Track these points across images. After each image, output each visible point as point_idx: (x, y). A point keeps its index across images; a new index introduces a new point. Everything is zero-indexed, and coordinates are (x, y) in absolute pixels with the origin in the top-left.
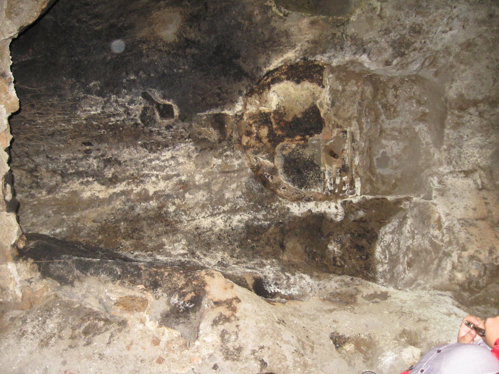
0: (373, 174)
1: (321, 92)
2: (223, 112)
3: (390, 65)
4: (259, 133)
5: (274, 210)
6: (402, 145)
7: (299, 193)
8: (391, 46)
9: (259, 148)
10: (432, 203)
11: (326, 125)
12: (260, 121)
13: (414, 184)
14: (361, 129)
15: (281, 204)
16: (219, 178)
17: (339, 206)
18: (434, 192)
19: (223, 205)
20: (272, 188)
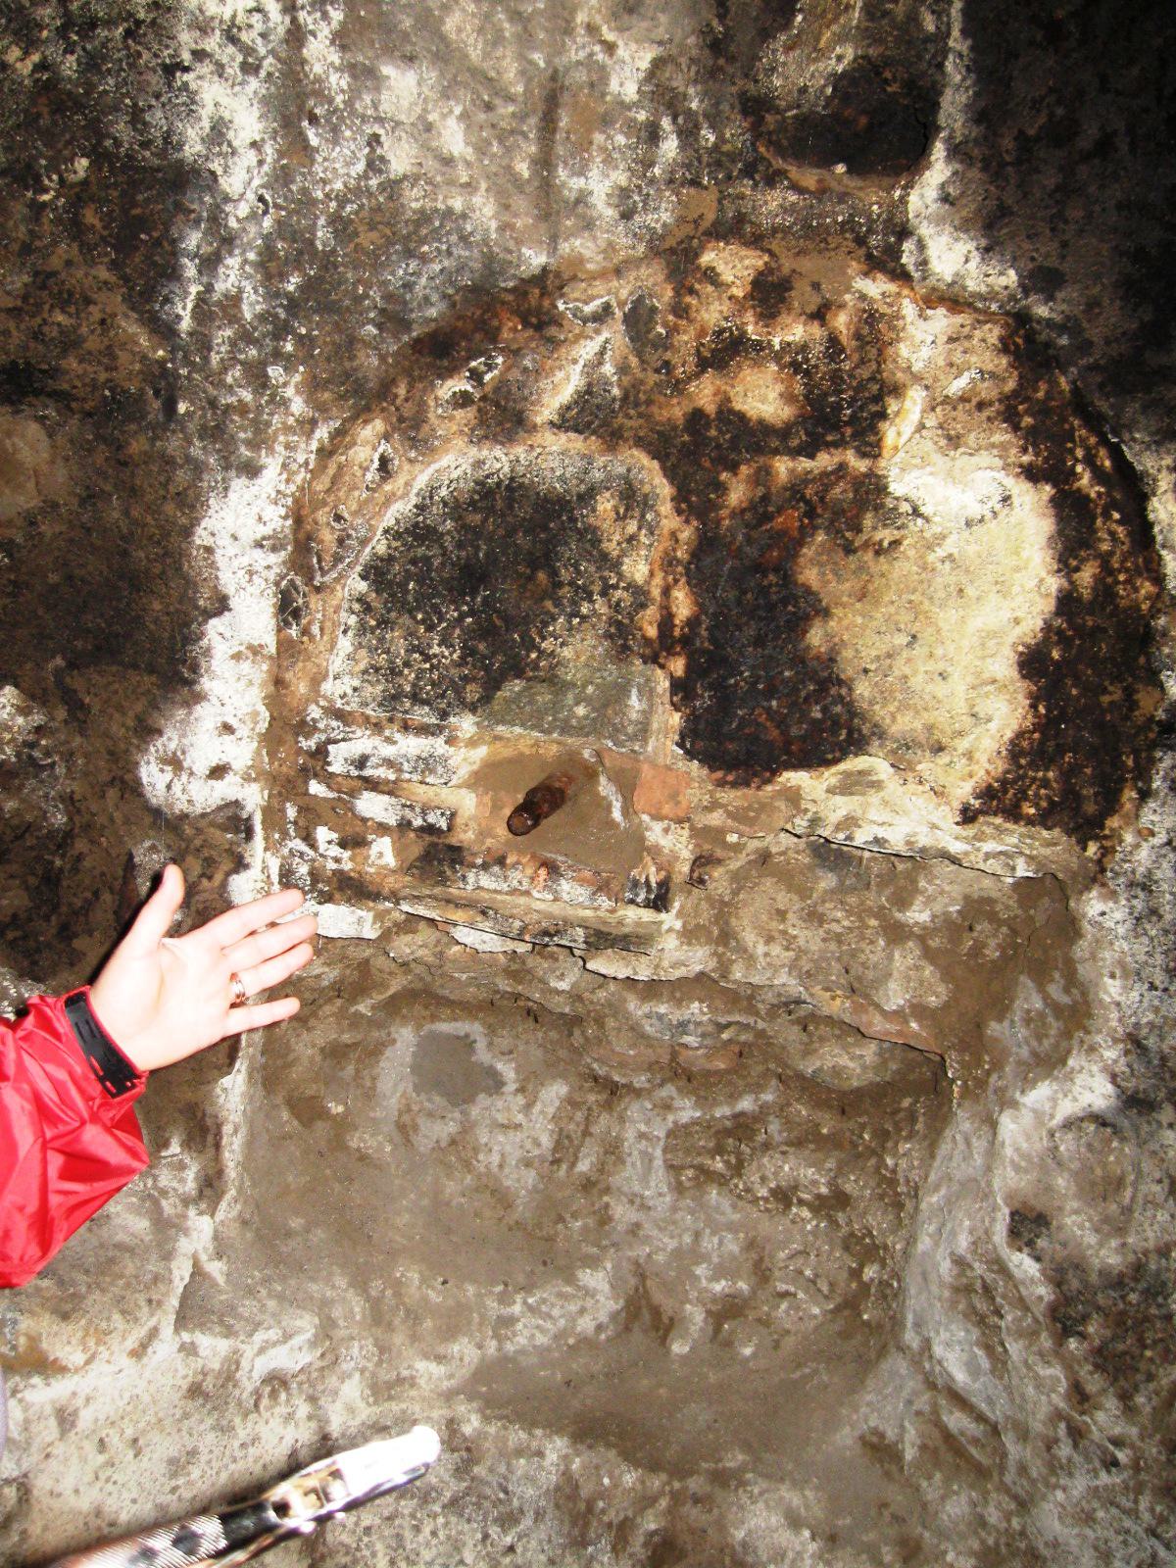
0: (393, 1007)
1: (938, 793)
2: (939, 151)
3: (1014, 1233)
4: (758, 364)
5: (257, 377)
6: (522, 1182)
7: (338, 559)
8: (1139, 1268)
9: (664, 343)
10: (154, 1333)
11: (731, 797)
12: (836, 377)
13: (296, 1223)
14: (651, 989)
15: (287, 429)
16: (521, 57)
17: (227, 789)
18: (223, 1346)
19: (341, 39)
20: (401, 390)
